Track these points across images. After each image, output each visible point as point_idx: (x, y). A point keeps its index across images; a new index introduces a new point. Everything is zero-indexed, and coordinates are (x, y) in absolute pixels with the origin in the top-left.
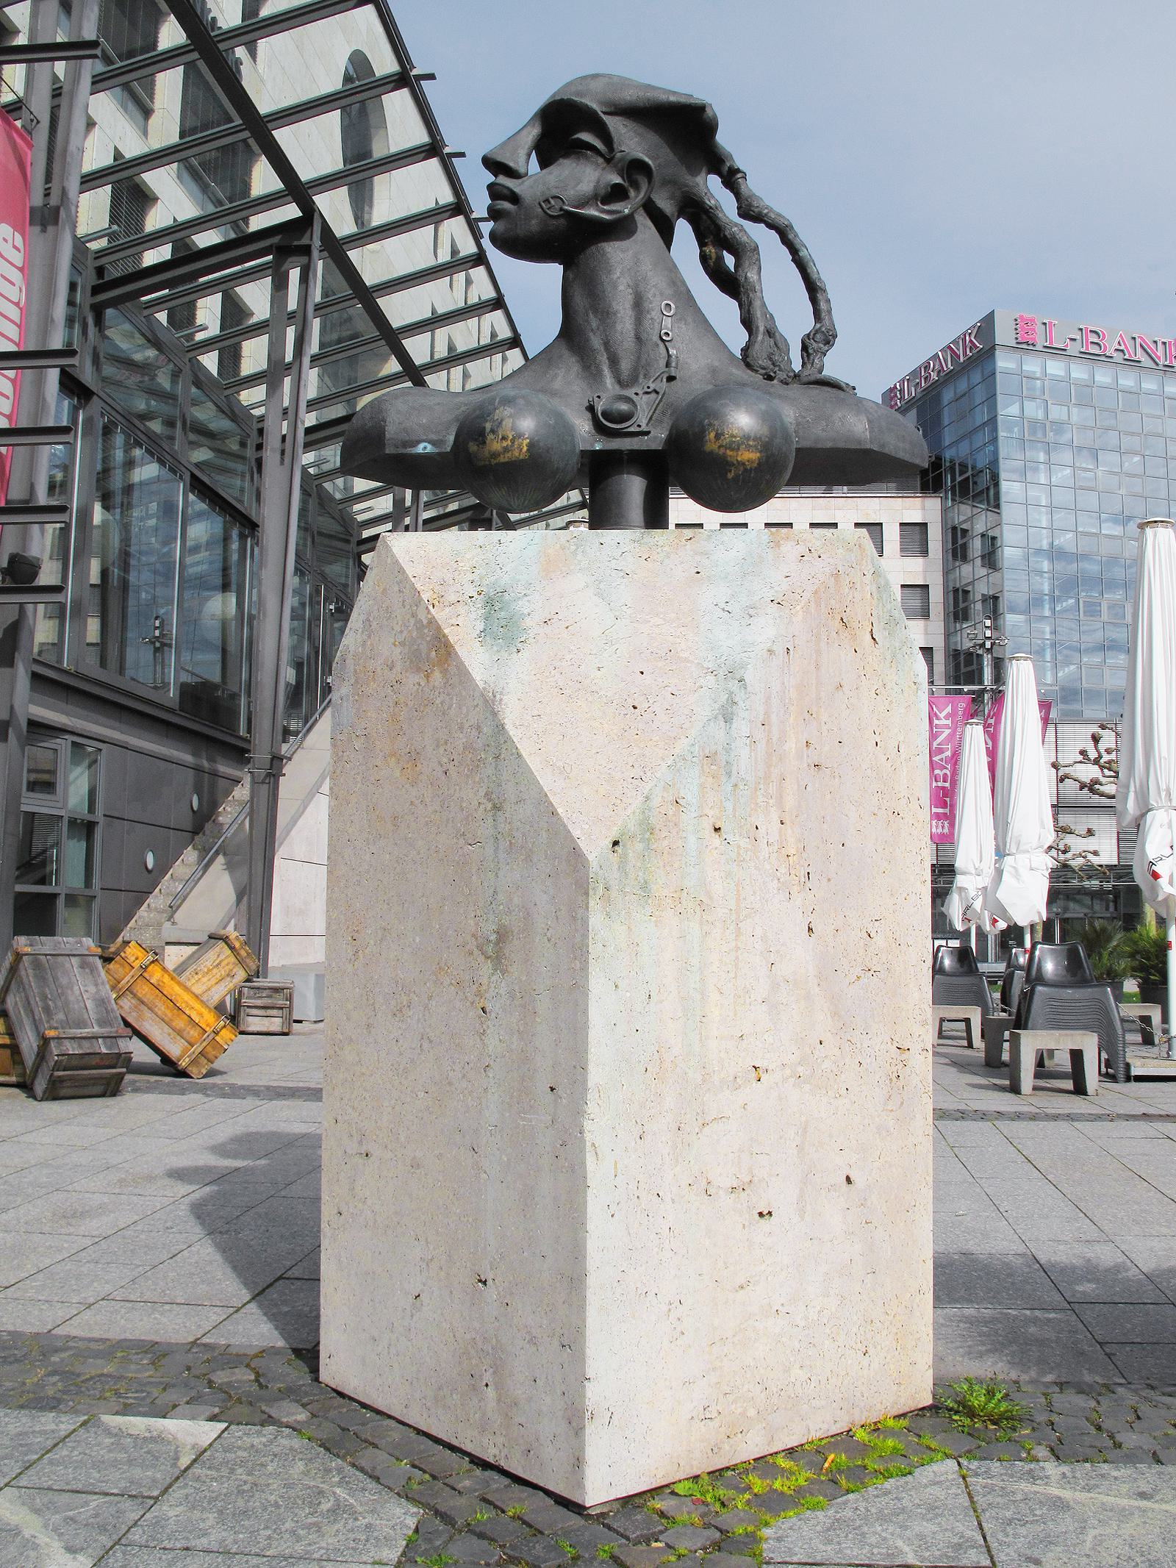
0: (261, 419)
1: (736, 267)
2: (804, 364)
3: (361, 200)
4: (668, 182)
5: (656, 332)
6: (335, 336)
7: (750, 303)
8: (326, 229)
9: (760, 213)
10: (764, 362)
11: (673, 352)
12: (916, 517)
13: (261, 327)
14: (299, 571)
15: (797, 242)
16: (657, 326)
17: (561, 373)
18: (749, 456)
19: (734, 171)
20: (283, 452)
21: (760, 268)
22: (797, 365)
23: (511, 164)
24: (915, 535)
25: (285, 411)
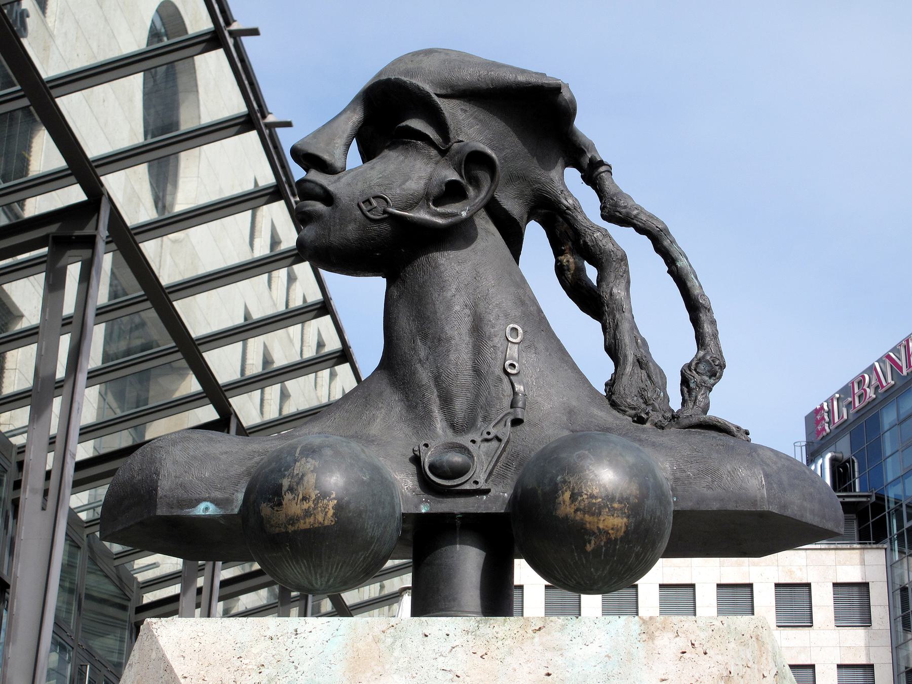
0: (22, 450)
1: (599, 280)
2: (684, 402)
3: (163, 182)
4: (513, 178)
5: (499, 363)
6: (123, 346)
7: (617, 326)
8: (116, 216)
9: (628, 215)
10: (633, 400)
11: (519, 388)
12: (853, 575)
13: (30, 335)
14: (59, 645)
15: (674, 250)
16: (500, 355)
17: (380, 414)
18: (615, 522)
19: (597, 164)
20: (46, 493)
21: (628, 282)
22: (675, 403)
23: (326, 157)
24: (853, 599)
25: (52, 441)
